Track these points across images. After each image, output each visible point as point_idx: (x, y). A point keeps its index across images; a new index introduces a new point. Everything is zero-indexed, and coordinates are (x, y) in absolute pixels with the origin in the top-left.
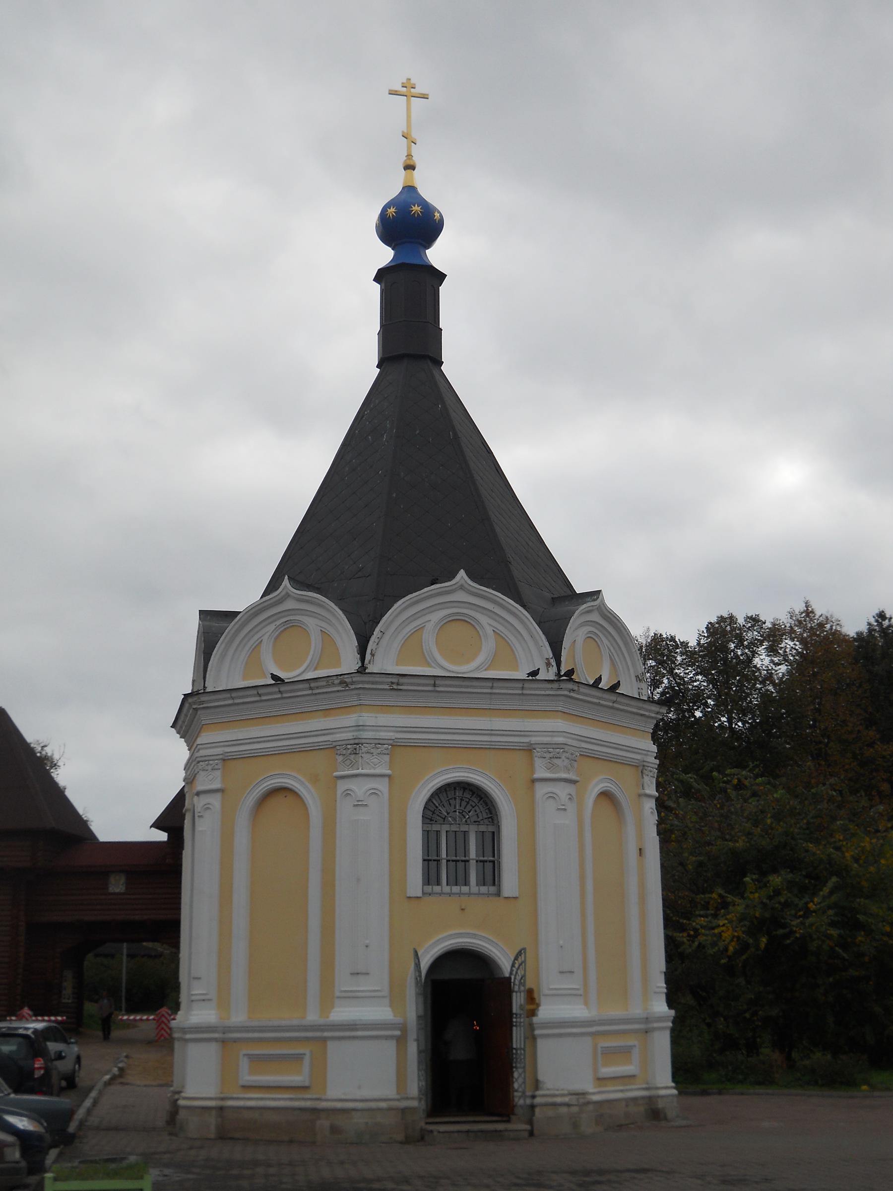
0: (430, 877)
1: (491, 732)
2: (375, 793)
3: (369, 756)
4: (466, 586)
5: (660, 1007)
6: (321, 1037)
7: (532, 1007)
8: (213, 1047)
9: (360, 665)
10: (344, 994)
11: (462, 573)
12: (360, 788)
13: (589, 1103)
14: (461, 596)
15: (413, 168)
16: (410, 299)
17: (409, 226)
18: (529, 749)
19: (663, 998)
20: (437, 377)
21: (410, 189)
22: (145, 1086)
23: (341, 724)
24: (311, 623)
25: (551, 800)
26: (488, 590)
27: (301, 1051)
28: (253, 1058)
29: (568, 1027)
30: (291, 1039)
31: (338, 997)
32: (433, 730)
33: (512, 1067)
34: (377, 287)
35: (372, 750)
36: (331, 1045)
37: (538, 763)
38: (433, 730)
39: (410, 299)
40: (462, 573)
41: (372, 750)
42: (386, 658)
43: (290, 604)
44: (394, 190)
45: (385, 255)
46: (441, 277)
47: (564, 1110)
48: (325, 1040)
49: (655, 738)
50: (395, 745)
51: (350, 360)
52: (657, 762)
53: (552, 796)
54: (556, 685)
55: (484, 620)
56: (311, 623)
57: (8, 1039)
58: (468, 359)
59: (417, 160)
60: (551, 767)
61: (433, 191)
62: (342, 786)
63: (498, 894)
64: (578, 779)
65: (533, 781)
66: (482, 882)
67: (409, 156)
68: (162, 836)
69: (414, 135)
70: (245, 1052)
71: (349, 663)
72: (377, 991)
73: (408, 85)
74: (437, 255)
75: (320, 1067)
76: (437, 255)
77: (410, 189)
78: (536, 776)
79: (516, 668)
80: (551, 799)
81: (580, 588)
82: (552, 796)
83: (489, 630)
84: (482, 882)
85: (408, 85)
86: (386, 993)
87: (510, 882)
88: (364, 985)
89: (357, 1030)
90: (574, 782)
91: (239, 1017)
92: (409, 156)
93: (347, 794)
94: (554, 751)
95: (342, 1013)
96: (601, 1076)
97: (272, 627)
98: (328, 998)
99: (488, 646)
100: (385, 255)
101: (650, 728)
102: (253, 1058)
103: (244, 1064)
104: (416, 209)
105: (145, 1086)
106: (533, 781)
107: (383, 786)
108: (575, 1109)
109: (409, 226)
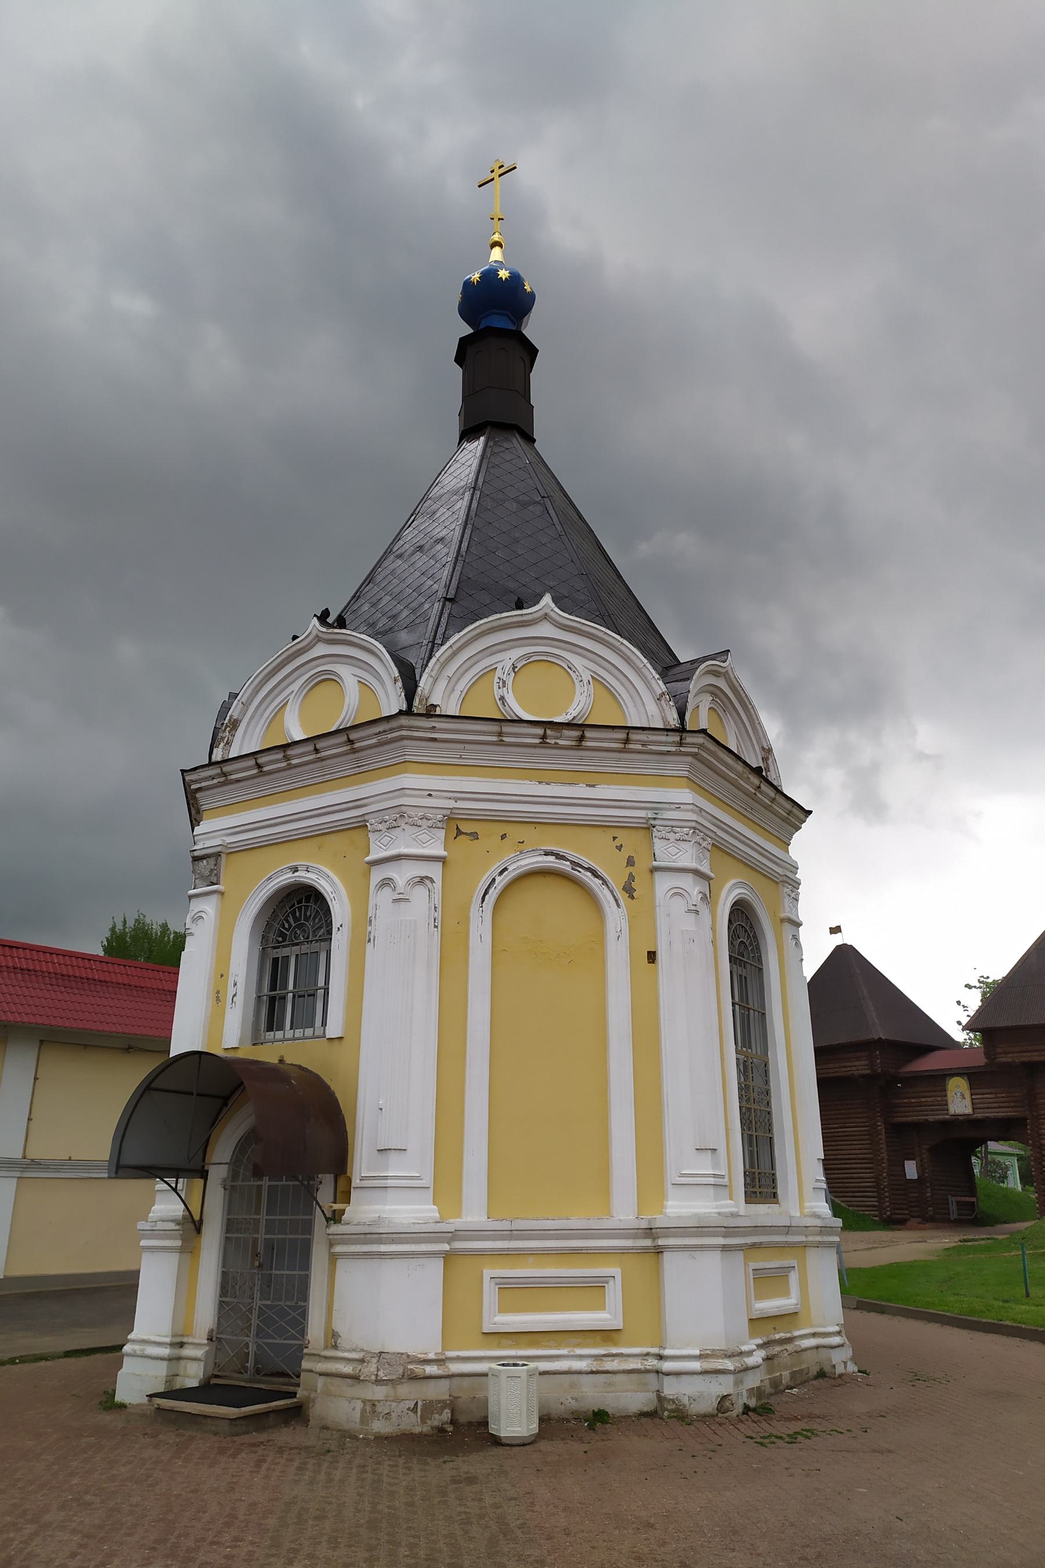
3: (664, 842)
4: (552, 614)
6: (652, 1244)
11: (547, 599)
12: (402, 874)
14: (546, 630)
22: (68, 1354)
25: (677, 898)
26: (491, 618)
27: (786, 1263)
28: (507, 1287)
30: (546, 1253)
32: (643, 805)
35: (669, 835)
36: (667, 1256)
38: (643, 805)
40: (547, 599)
41: (669, 835)
48: (659, 1251)
53: (679, 893)
55: (576, 661)
56: (348, 675)
57: (697, 1254)
62: (377, 875)
64: (712, 875)
71: (392, 701)
80: (677, 897)
86: (428, 1181)
89: (380, 1242)
91: (474, 1214)
93: (386, 883)
95: (680, 1207)
102: (507, 1287)
103: (490, 1294)
105: (68, 1354)
107: (434, 871)
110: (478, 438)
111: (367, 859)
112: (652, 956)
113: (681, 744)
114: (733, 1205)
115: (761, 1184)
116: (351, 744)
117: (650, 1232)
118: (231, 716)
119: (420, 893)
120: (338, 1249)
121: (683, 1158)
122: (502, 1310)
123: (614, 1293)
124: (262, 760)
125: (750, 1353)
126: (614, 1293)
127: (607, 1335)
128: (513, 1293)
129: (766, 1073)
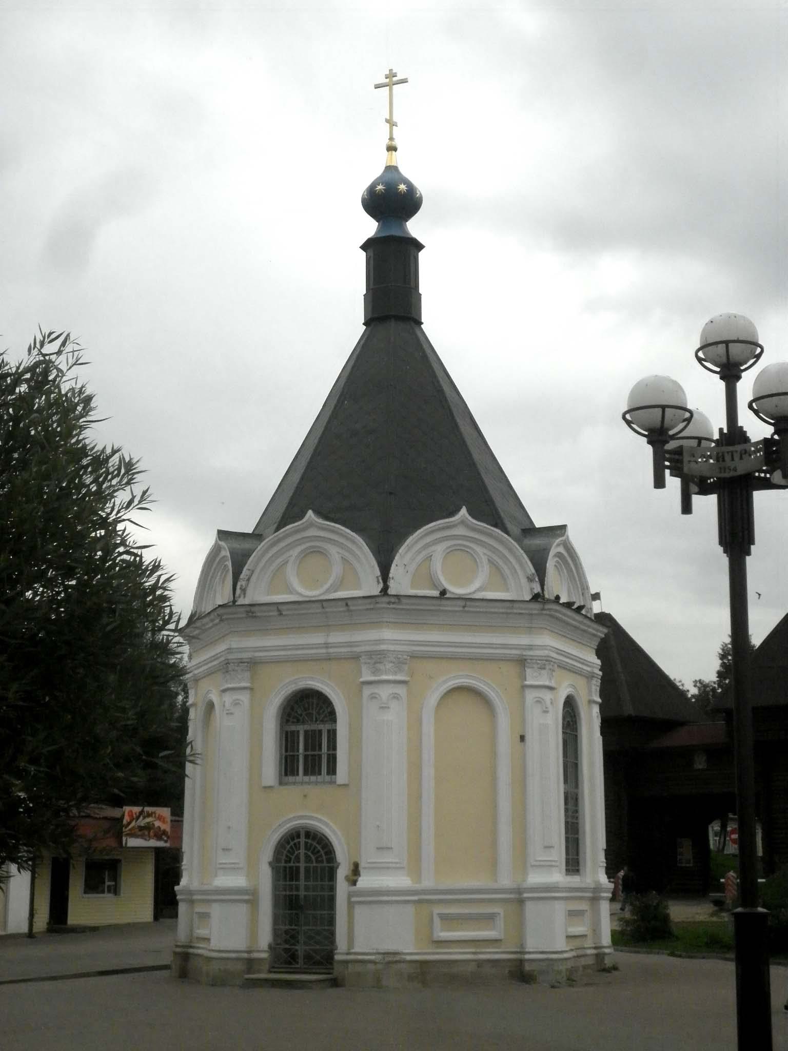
0: (288, 767)
2: (396, 697)
5: (603, 878)
6: (518, 899)
7: (355, 878)
8: (410, 910)
9: (381, 585)
10: (538, 863)
11: (464, 511)
12: (384, 692)
13: (404, 961)
14: (461, 531)
15: (395, 149)
16: (392, 267)
17: (392, 203)
18: (356, 657)
19: (603, 870)
20: (419, 334)
23: (365, 637)
24: (333, 551)
27: (496, 910)
29: (384, 895)
31: (532, 866)
33: (694, 923)
34: (363, 255)
37: (364, 669)
39: (392, 267)
40: (464, 511)
42: (402, 580)
43: (312, 532)
44: (377, 171)
45: (369, 227)
46: (419, 246)
47: (371, 967)
49: (599, 654)
52: (601, 673)
54: (438, 602)
55: (479, 549)
56: (333, 551)
59: (397, 143)
60: (375, 672)
61: (416, 173)
62: (367, 691)
63: (333, 782)
65: (524, 687)
66: (328, 773)
67: (391, 139)
69: (395, 119)
70: (438, 911)
72: (396, 863)
73: (391, 75)
74: (415, 227)
75: (520, 924)
76: (415, 227)
78: (527, 683)
79: (358, 586)
81: (539, 521)
82: (539, 701)
83: (485, 560)
84: (328, 773)
85: (391, 75)
87: (342, 774)
88: (388, 858)
90: (551, 688)
91: (428, 882)
92: (391, 139)
93: (373, 697)
94: (545, 663)
95: (535, 878)
96: (435, 938)
97: (298, 549)
99: (337, 570)
100: (369, 227)
101: (595, 644)
102: (444, 917)
104: (402, 187)
106: (524, 687)
107: (401, 690)
108: (379, 967)
109: (392, 203)
110: (598, 658)
111: (361, 680)
112: (522, 738)
113: (543, 609)
114: (558, 877)
115: (573, 864)
116: (348, 611)
117: (519, 891)
118: (712, 915)
119: (394, 705)
120: (353, 899)
121: (537, 854)
122: (442, 930)
123: (500, 922)
124: (280, 607)
125: (25, 851)
126: (500, 922)
127: (496, 941)
128: (448, 920)
129: (577, 799)
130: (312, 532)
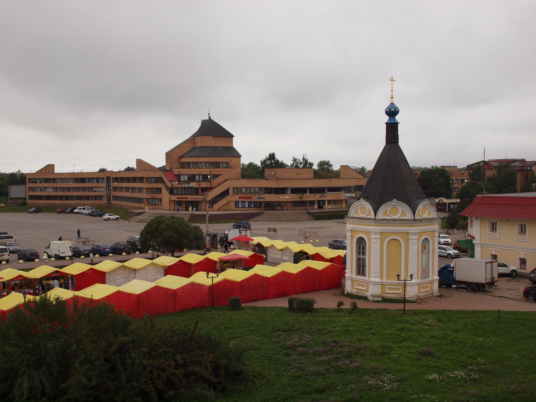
1: (195, 198)
5: (437, 277)
15: (392, 98)
16: (392, 130)
17: (392, 112)
21: (392, 104)
24: (400, 208)
28: (357, 284)
39: (392, 130)
44: (388, 104)
50: (381, 233)
51: (382, 143)
56: (400, 208)
58: (402, 143)
68: (346, 293)
76: (398, 118)
77: (392, 104)
95: (372, 279)
98: (369, 278)
100: (386, 118)
102: (357, 284)
103: (356, 285)
109: (392, 112)
130: (362, 203)
